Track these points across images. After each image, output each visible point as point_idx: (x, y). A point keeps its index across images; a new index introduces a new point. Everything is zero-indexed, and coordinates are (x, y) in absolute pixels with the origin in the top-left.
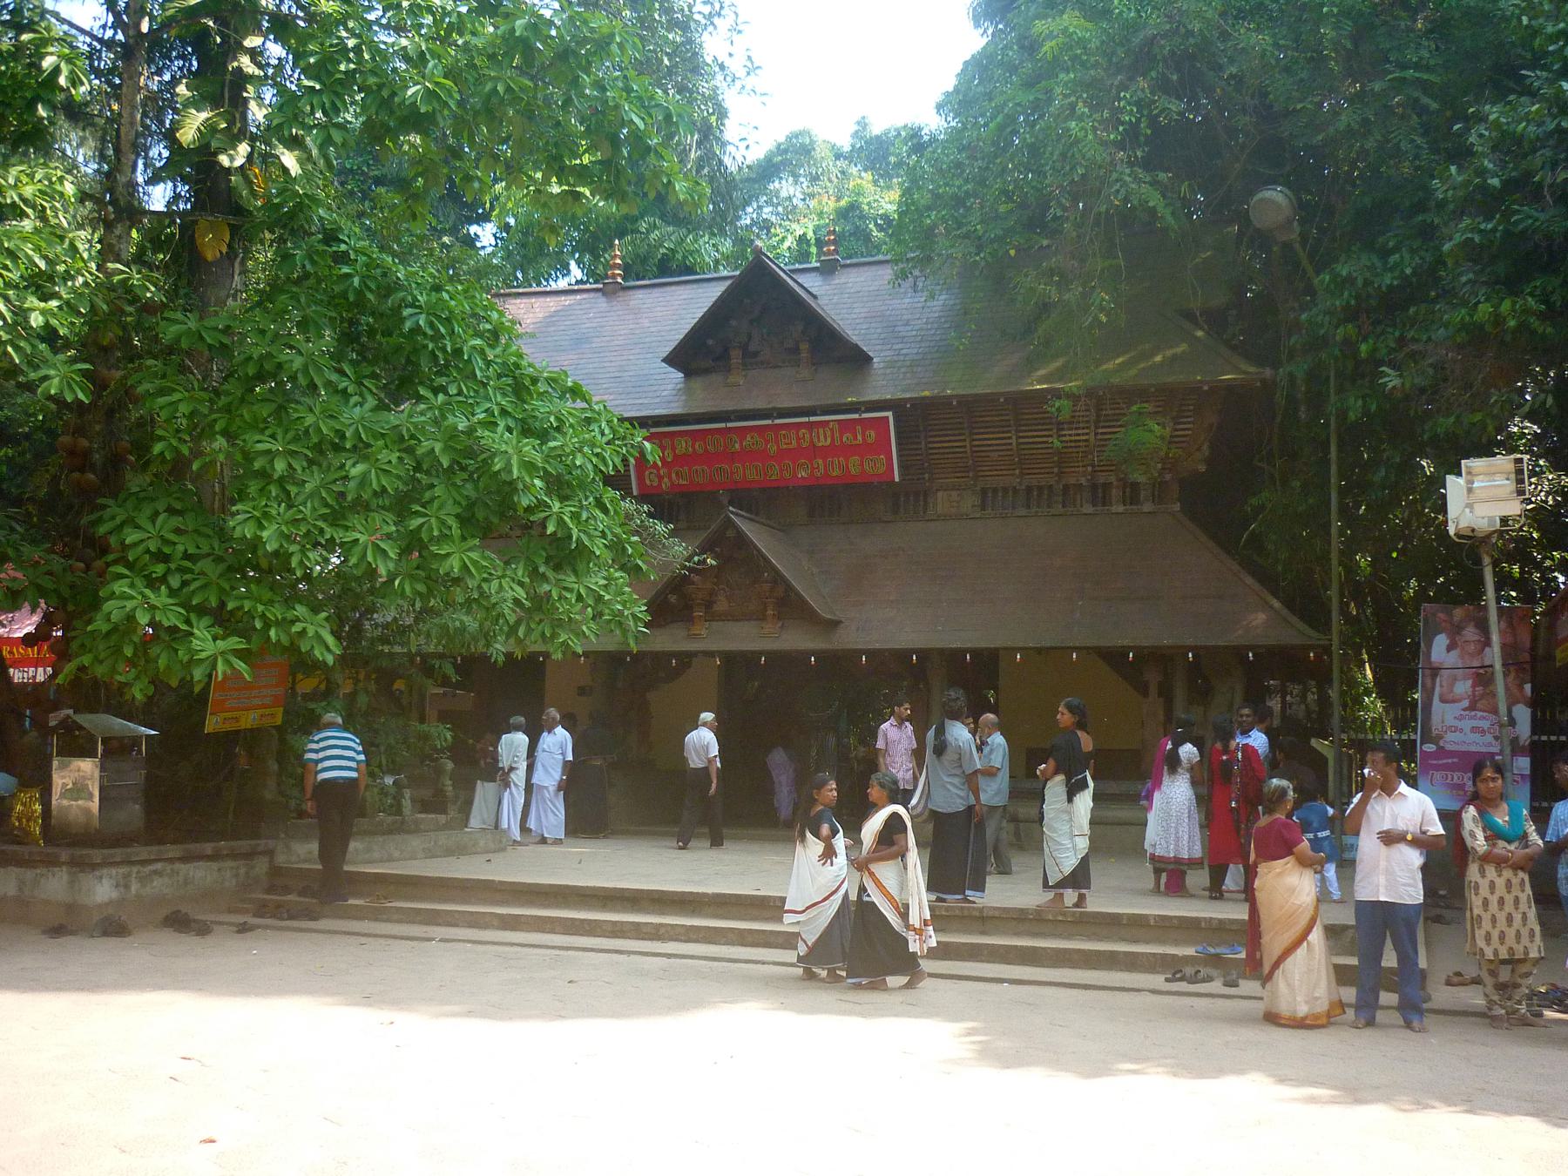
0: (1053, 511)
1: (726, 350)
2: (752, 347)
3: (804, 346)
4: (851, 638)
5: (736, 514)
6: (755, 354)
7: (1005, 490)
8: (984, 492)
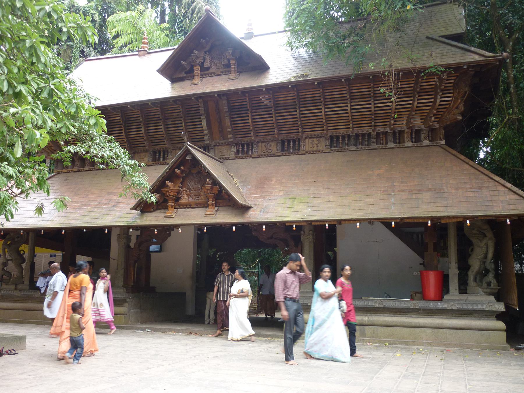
0: (372, 147)
1: (192, 67)
2: (206, 65)
3: (233, 62)
4: (255, 216)
5: (189, 145)
6: (208, 69)
8: (332, 138)
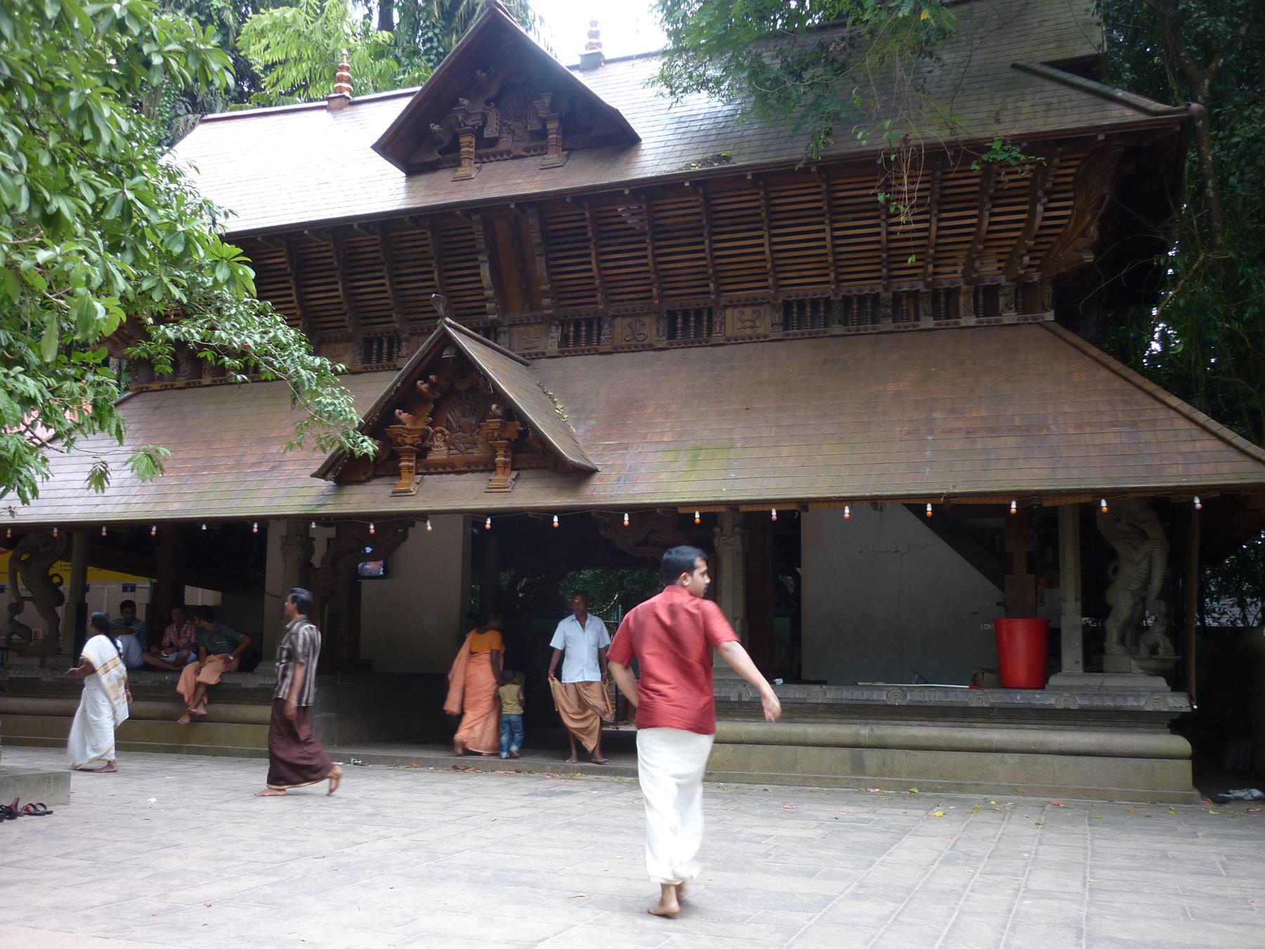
2: (489, 132)
3: (552, 126)
6: (493, 142)
7: (815, 304)
8: (787, 306)
